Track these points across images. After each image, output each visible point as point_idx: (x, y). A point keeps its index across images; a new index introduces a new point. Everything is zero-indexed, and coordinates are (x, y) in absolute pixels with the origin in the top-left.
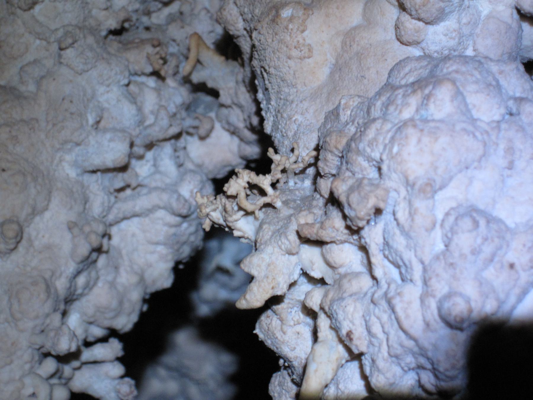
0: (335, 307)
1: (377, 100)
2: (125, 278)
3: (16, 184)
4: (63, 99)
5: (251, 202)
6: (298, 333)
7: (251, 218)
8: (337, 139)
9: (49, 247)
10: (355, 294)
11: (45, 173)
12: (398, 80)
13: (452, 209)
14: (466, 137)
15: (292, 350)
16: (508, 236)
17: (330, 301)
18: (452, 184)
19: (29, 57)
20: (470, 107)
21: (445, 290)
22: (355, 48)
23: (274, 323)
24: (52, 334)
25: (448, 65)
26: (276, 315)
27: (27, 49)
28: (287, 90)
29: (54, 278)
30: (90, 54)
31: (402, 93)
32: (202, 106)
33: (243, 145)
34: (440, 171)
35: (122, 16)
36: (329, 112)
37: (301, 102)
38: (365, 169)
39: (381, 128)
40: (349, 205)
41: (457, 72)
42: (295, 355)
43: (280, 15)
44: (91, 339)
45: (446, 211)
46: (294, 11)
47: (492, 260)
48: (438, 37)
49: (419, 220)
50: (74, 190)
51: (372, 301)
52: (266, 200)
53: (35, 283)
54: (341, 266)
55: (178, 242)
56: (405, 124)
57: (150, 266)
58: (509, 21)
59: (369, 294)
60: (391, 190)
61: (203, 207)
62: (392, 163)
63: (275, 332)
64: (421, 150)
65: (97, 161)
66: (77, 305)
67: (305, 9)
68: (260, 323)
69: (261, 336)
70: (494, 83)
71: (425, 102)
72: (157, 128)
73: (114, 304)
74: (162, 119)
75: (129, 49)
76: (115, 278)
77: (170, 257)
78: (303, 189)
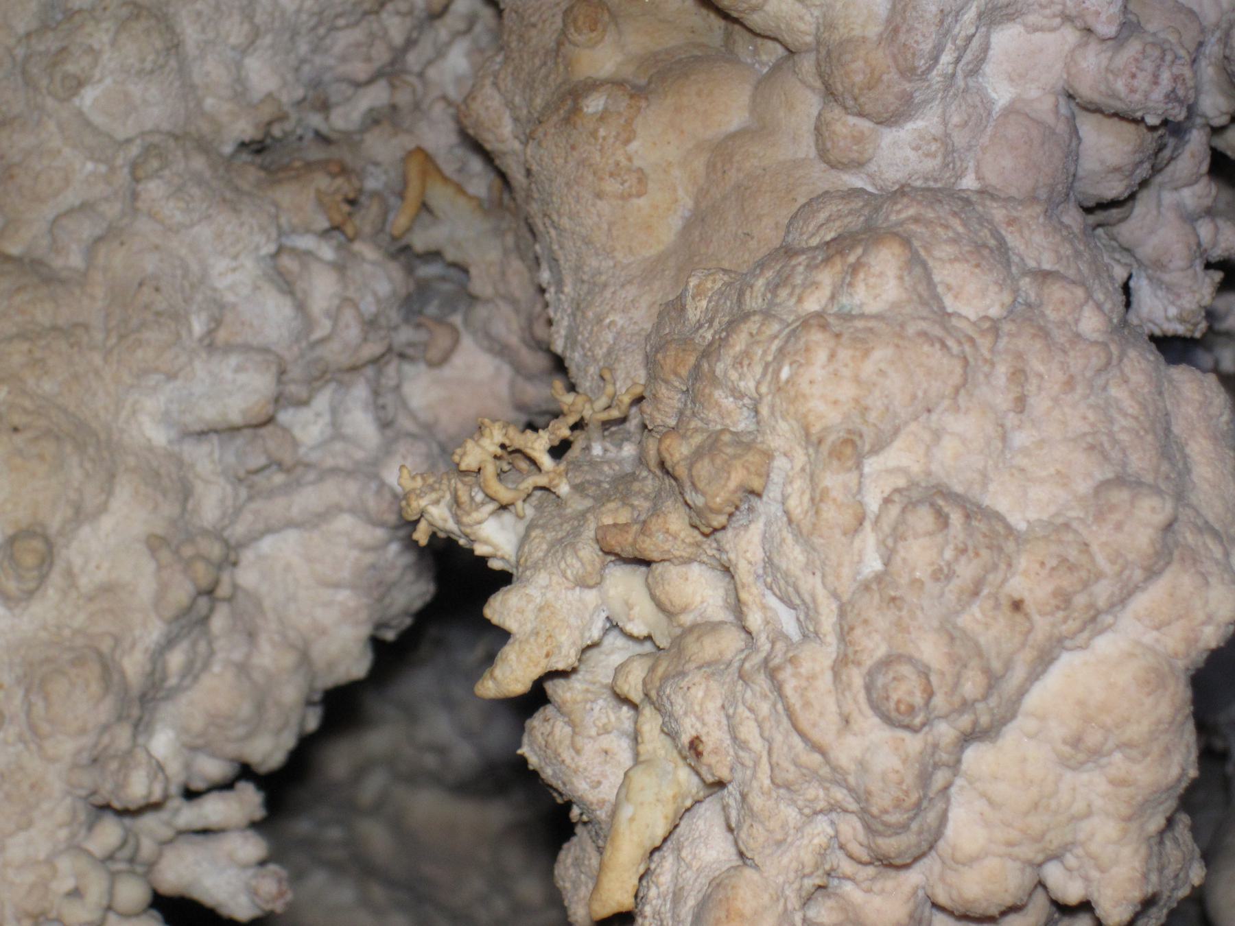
0: (668, 691)
1: (757, 277)
2: (269, 656)
3: (41, 457)
4: (141, 285)
5: (510, 486)
6: (606, 753)
7: (507, 517)
8: (677, 355)
9: (108, 588)
10: (709, 664)
11: (103, 436)
12: (805, 237)
13: (897, 490)
14: (926, 348)
15: (594, 788)
16: (1010, 546)
17: (661, 679)
18: (898, 444)
19: (71, 198)
20: (940, 289)
21: (882, 651)
22: (734, 176)
23: (557, 731)
24: (114, 765)
25: (899, 207)
26: (562, 714)
27: (67, 181)
28: (594, 263)
29: (118, 652)
30: (196, 191)
31: (805, 263)
32: (436, 302)
33: (520, 382)
34: (873, 416)
35: (267, 112)
36: (667, 304)
37: (623, 286)
38: (729, 413)
39: (759, 332)
40: (693, 484)
41: (916, 220)
42: (601, 796)
43: (581, 110)
44: (197, 785)
45: (885, 495)
46: (610, 102)
47: (976, 593)
48: (900, 152)
49: (829, 513)
50: (163, 471)
51: (741, 677)
52: (542, 480)
53: (79, 661)
54: (684, 610)
55: (380, 583)
56: (806, 322)
57: (323, 632)
58: (1050, 119)
59: (736, 664)
60: (776, 454)
61: (413, 497)
62: (778, 401)
63: (560, 750)
64: (836, 373)
65: (210, 413)
66: (167, 711)
67: (632, 97)
68: (530, 734)
69: (534, 761)
70: (992, 243)
71: (848, 279)
72: (335, 346)
73: (246, 709)
74: (347, 326)
75: (279, 181)
76: (248, 656)
77: (363, 615)
78: (620, 462)
